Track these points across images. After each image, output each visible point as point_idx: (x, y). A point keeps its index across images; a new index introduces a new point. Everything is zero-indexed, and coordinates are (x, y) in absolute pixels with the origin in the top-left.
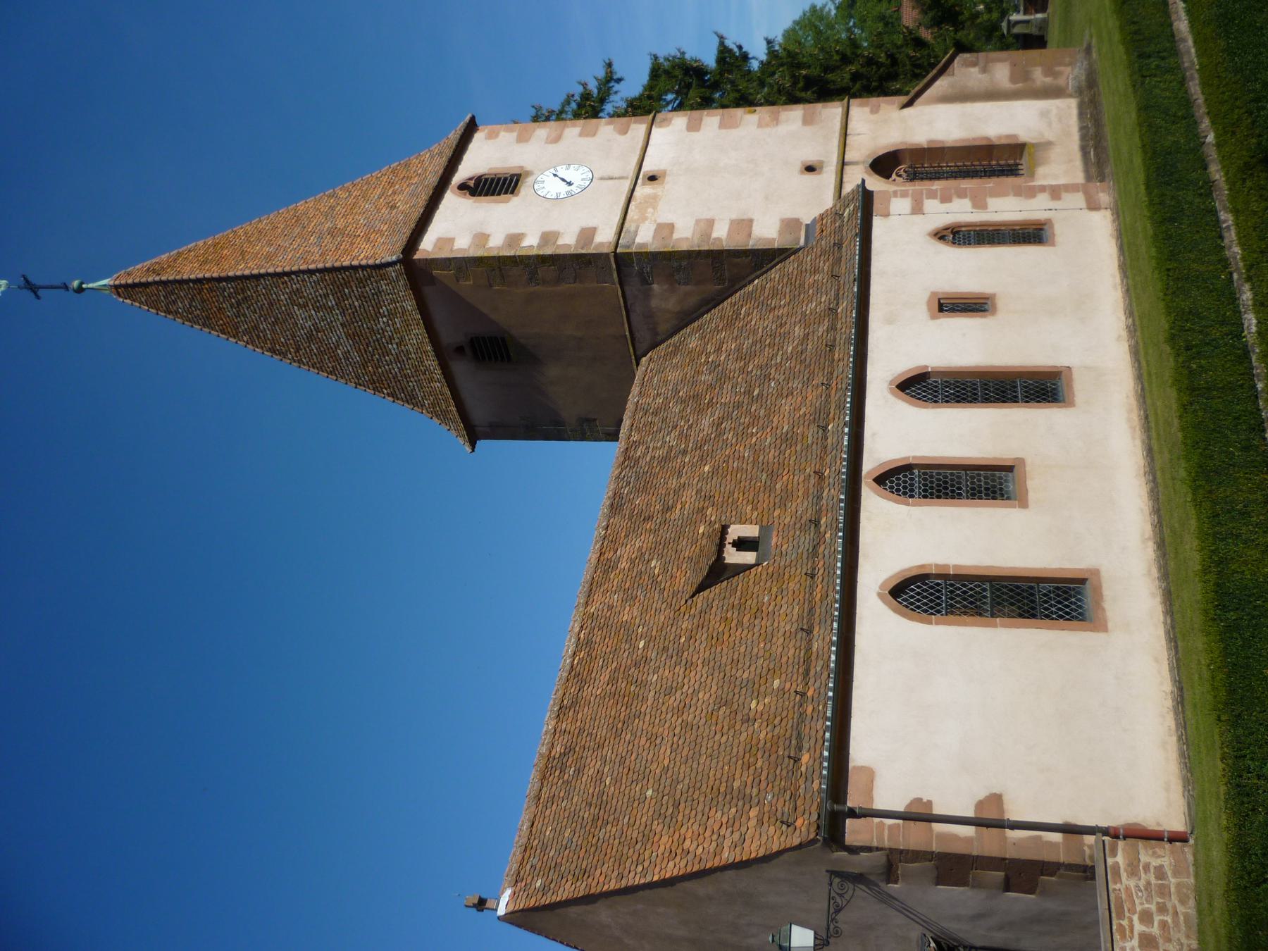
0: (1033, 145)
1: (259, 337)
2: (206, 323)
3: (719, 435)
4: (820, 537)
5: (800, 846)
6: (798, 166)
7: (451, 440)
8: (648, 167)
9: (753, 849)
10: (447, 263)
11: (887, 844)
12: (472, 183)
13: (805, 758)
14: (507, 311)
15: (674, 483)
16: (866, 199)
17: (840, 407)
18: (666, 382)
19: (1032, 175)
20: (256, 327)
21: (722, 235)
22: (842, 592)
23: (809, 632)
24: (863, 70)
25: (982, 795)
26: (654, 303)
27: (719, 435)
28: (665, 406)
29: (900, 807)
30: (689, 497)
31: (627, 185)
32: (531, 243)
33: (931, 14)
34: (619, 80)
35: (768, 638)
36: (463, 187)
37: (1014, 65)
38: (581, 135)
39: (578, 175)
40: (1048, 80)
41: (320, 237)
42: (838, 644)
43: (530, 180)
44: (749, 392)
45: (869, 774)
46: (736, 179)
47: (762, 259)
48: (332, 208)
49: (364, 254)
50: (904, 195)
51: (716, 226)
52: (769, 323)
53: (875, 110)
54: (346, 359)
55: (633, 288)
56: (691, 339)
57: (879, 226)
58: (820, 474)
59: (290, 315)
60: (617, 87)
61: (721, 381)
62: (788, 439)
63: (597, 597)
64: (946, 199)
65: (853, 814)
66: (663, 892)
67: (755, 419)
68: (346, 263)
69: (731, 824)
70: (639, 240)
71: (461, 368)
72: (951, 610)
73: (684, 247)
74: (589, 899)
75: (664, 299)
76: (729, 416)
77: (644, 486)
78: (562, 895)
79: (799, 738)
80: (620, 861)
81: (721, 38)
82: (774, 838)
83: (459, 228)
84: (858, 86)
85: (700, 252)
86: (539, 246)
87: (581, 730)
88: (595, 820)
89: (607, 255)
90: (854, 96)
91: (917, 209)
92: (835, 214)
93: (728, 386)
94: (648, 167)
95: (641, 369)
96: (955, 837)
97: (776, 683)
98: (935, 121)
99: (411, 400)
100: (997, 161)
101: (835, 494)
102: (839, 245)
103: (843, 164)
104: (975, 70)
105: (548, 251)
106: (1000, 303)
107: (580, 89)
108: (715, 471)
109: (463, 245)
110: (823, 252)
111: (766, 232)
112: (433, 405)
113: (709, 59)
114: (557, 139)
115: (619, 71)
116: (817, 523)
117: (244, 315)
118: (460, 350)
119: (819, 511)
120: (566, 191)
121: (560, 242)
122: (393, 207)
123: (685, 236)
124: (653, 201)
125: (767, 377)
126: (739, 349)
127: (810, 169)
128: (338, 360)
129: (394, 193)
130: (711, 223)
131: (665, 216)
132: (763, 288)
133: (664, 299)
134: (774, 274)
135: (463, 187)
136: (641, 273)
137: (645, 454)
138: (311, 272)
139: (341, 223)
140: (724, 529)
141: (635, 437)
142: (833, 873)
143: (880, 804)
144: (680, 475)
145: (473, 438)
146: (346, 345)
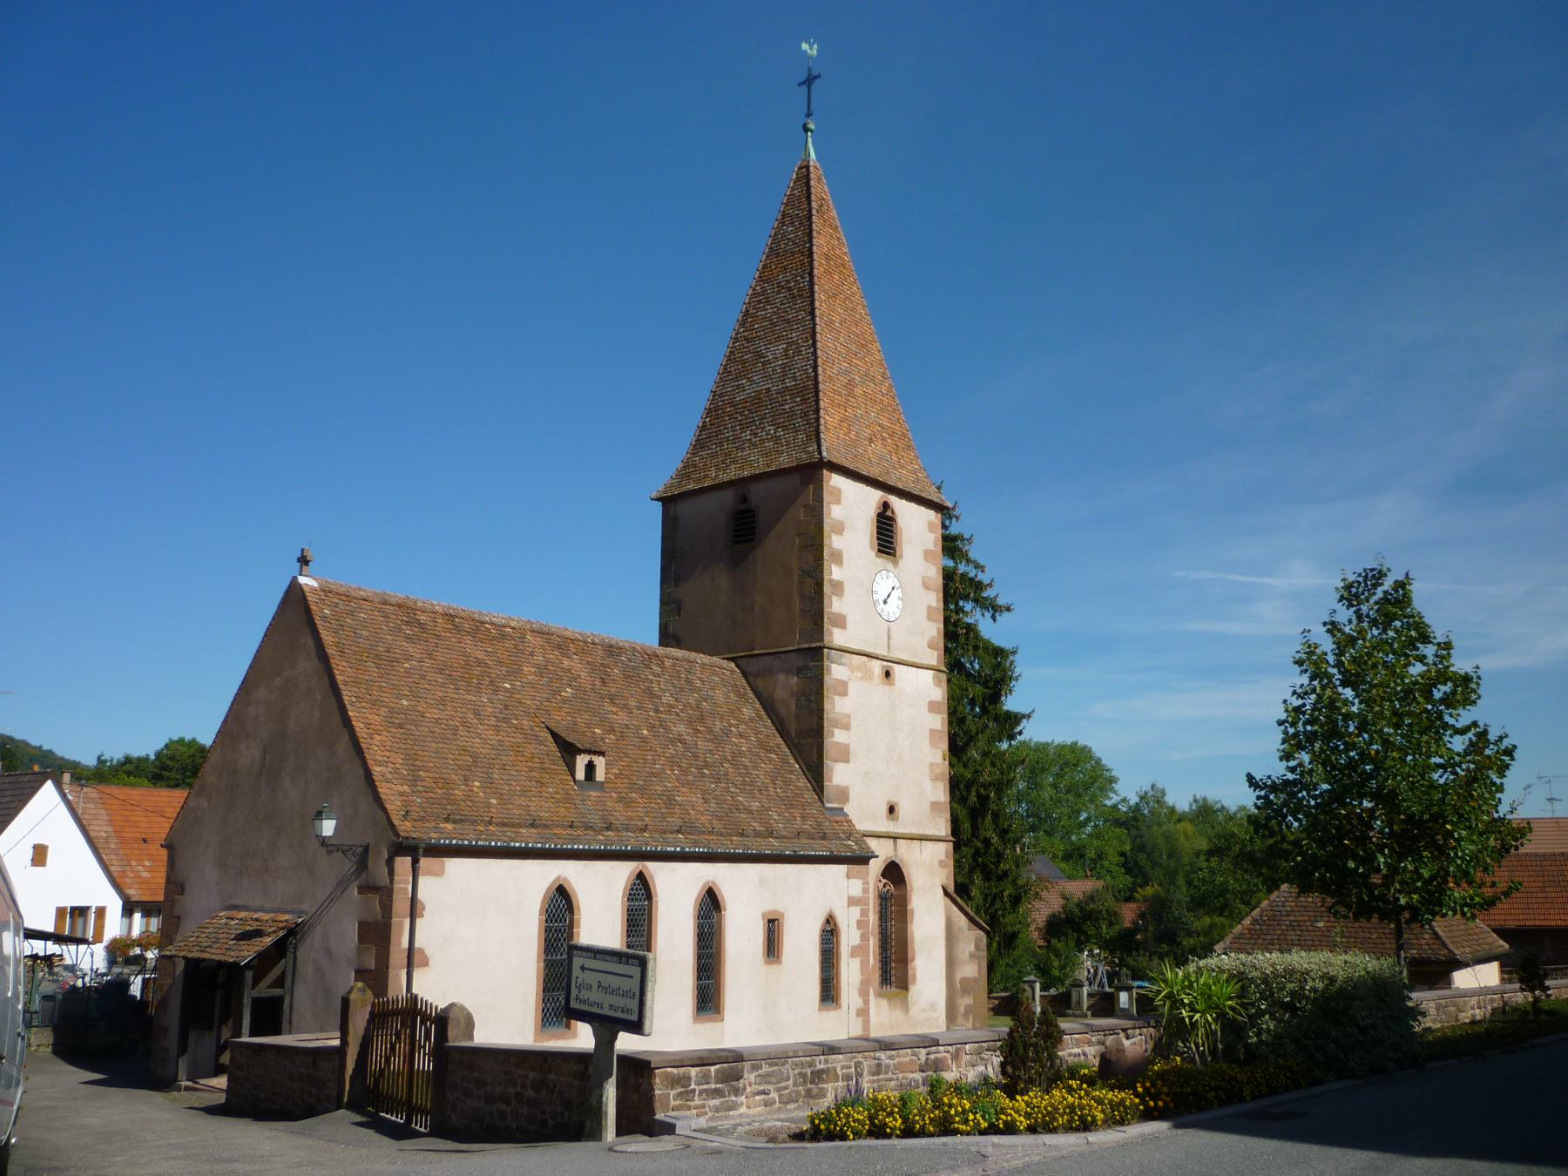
0: (906, 998)
1: (759, 302)
2: (773, 252)
3: (672, 741)
4: (599, 832)
5: (392, 826)
6: (894, 800)
7: (663, 464)
8: (898, 670)
9: (384, 790)
10: (819, 499)
11: (396, 886)
12: (889, 513)
13: (449, 826)
14: (776, 546)
15: (632, 703)
16: (861, 859)
17: (696, 844)
18: (713, 688)
19: (879, 995)
20: (768, 302)
21: (836, 737)
22: (561, 849)
23: (533, 825)
24: (992, 850)
25: (428, 952)
26: (782, 677)
27: (672, 741)
28: (695, 690)
29: (421, 895)
30: (621, 718)
31: (882, 652)
32: (834, 573)
33: (1076, 910)
34: (994, 618)
35: (524, 793)
36: (886, 505)
37: (975, 980)
38: (929, 607)
39: (893, 609)
40: (962, 1009)
41: (846, 373)
42: (526, 848)
43: (890, 566)
44: (707, 765)
45: (439, 873)
46: (888, 745)
47: (815, 772)
48: (873, 380)
49: (830, 418)
50: (865, 890)
51: (844, 732)
52: (762, 779)
53: (942, 864)
54: (738, 387)
55: (798, 661)
56: (751, 710)
57: (840, 870)
58: (645, 829)
59: (778, 339)
60: (988, 615)
61: (715, 739)
62: (670, 801)
63: (539, 641)
64: (860, 924)
65: (415, 862)
66: (337, 718)
67: (685, 772)
68: (822, 404)
69: (396, 771)
70: (834, 666)
71: (728, 498)
72: (548, 930)
73: (827, 707)
74: (324, 658)
75: (785, 685)
76: (687, 749)
77: (630, 677)
78: (324, 633)
79: (461, 821)
80: (357, 683)
81: (1028, 716)
82: (394, 806)
83: (849, 507)
84: (979, 844)
85: (822, 719)
86: (831, 581)
87: (438, 637)
88: (378, 657)
89: (822, 640)
90: (957, 847)
91: (852, 901)
92: (851, 833)
93: (711, 746)
94: (898, 670)
95: (725, 663)
96: (401, 934)
97: (494, 801)
98: (931, 915)
99: (699, 445)
100: (893, 967)
101: (631, 842)
102: (824, 837)
103: (895, 838)
104: (972, 948)
105: (827, 589)
106: (774, 967)
107: (986, 582)
108: (644, 739)
109: (834, 512)
110: (819, 824)
111: (838, 775)
112: (695, 466)
113: (1011, 703)
114: (926, 586)
115: (1003, 618)
116: (608, 829)
117: (779, 292)
118: (744, 500)
119: (617, 830)
120: (880, 601)
121: (834, 599)
122: (871, 441)
123: (836, 706)
124: (868, 676)
125: (718, 781)
126: (741, 754)
127: (892, 810)
128: (736, 379)
129: (884, 439)
130: (847, 727)
131: (853, 689)
132: (791, 772)
133: (785, 685)
134: (803, 782)
135: (886, 505)
136: (807, 668)
137: (654, 674)
138: (815, 368)
139: (858, 391)
140: (602, 754)
141: (668, 663)
142: (366, 849)
143: (422, 881)
144: (639, 708)
145: (667, 501)
146: (751, 390)
